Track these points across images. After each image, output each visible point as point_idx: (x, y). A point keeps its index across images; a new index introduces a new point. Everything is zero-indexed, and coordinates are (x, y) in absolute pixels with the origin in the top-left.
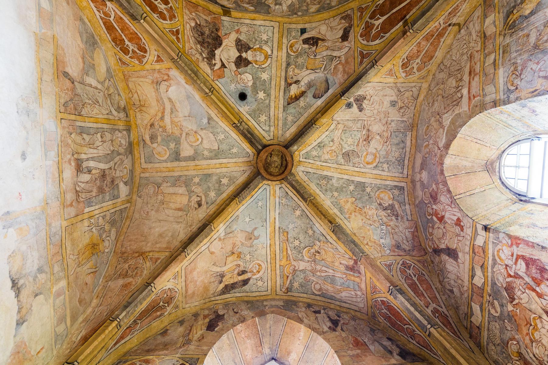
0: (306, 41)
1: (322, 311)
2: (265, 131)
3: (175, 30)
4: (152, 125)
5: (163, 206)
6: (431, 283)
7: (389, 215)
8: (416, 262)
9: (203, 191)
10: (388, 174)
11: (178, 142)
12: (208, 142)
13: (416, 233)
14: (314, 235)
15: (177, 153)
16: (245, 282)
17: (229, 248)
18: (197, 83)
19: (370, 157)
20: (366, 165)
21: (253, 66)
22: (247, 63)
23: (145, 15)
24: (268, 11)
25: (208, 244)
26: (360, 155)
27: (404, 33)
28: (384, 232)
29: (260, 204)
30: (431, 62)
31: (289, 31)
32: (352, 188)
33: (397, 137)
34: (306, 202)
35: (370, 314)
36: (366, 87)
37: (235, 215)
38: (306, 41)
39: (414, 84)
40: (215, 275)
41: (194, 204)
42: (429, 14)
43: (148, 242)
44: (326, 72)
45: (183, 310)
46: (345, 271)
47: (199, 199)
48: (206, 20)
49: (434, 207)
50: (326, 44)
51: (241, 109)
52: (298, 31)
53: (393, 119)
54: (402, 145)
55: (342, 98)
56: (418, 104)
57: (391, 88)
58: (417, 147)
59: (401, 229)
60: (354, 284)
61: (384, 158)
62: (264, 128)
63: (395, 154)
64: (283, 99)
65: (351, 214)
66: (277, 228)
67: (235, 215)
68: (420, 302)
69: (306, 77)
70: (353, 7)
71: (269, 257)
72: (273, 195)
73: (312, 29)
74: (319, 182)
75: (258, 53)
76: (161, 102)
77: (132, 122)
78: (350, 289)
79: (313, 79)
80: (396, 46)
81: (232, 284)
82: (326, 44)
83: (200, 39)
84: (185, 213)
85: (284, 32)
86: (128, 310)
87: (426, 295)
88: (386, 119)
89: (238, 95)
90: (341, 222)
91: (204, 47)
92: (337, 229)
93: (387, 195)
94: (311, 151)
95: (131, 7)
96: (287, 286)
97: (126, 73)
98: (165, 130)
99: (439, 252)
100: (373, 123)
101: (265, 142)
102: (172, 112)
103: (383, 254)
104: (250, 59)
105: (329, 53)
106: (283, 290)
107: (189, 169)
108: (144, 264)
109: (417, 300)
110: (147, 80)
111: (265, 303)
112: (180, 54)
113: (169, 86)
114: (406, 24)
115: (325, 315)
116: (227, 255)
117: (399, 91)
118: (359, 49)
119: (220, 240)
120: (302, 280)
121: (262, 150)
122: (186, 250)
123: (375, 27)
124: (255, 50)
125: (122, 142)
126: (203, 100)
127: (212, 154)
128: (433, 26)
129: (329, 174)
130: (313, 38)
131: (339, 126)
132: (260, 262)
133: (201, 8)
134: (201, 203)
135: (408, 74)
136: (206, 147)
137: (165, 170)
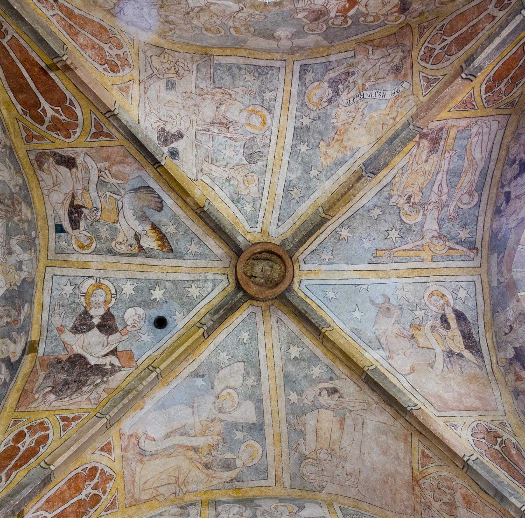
0: (75, 225)
1: (507, 189)
2: (215, 288)
3: (62, 423)
4: (207, 466)
5: (337, 450)
6: (454, 15)
8: (422, 40)
9: (311, 386)
10: (281, 90)
11: (236, 426)
12: (233, 376)
13: (376, 42)
14: (381, 206)
15: (251, 428)
16: (460, 317)
17: (405, 343)
18: (142, 391)
19: (254, 119)
20: (266, 126)
21: (113, 307)
22: (108, 316)
23: (42, 464)
24: (30, 283)
25: (398, 375)
26: (251, 136)
27: (67, 68)
28: (373, 93)
29: (331, 294)
31: (59, 251)
32: (303, 148)
33: (222, 78)
34: (327, 220)
36: (146, 127)
37: (351, 333)
38: (75, 225)
39: (142, 55)
40: (449, 366)
42: (40, 31)
43: (397, 472)
44: (123, 192)
45: (508, 414)
46: (439, 153)
47: (325, 392)
48: (45, 378)
49: (333, 14)
50: (79, 192)
52: (59, 237)
53: (194, 85)
54: (235, 70)
55: (163, 164)
56: (170, 46)
57: (147, 89)
58: (238, 45)
59: (369, 66)
60: (460, 139)
61: (255, 98)
62: (210, 290)
63: (248, 80)
64: (163, 260)
65: (345, 147)
66: (371, 267)
67: (351, 333)
68: (486, 29)
69: (129, 223)
70: (24, 151)
71: (419, 279)
72: (317, 273)
73: (56, 215)
74: (295, 201)
75: (93, 299)
76: (172, 451)
77: (204, 497)
78: (469, 145)
79: (132, 211)
80: (87, 81)
81: (464, 338)
83: (74, 387)
84: (348, 414)
85: (61, 259)
86: (507, 495)
88: (195, 97)
89: (159, 330)
90: (360, 162)
91: (87, 380)
92: (372, 168)
93: (315, 91)
94: (244, 214)
95: (32, 482)
96: (465, 249)
97: (127, 502)
98: (215, 447)
99: (404, 4)
100: (200, 117)
101: (231, 288)
102: (186, 434)
103: (409, 92)
104: (102, 311)
105: (92, 187)
106: (472, 255)
107: (276, 408)
108: (432, 476)
109: (483, 35)
110: (138, 470)
111: (495, 284)
112: (98, 415)
113: (147, 437)
114: (53, 67)
115: (512, 184)
116: (416, 346)
117: (151, 77)
118: (89, 140)
119: (390, 357)
120: (455, 224)
121: (245, 291)
122: (409, 409)
123: (56, 115)
124: (88, 304)
125: (235, 512)
126: (168, 384)
127: (252, 372)
128: (56, 27)
129: (281, 184)
130: (70, 213)
131: (206, 169)
132: (428, 293)
133: (27, 385)
134: (331, 389)
135: (126, 63)
137: (278, 448)
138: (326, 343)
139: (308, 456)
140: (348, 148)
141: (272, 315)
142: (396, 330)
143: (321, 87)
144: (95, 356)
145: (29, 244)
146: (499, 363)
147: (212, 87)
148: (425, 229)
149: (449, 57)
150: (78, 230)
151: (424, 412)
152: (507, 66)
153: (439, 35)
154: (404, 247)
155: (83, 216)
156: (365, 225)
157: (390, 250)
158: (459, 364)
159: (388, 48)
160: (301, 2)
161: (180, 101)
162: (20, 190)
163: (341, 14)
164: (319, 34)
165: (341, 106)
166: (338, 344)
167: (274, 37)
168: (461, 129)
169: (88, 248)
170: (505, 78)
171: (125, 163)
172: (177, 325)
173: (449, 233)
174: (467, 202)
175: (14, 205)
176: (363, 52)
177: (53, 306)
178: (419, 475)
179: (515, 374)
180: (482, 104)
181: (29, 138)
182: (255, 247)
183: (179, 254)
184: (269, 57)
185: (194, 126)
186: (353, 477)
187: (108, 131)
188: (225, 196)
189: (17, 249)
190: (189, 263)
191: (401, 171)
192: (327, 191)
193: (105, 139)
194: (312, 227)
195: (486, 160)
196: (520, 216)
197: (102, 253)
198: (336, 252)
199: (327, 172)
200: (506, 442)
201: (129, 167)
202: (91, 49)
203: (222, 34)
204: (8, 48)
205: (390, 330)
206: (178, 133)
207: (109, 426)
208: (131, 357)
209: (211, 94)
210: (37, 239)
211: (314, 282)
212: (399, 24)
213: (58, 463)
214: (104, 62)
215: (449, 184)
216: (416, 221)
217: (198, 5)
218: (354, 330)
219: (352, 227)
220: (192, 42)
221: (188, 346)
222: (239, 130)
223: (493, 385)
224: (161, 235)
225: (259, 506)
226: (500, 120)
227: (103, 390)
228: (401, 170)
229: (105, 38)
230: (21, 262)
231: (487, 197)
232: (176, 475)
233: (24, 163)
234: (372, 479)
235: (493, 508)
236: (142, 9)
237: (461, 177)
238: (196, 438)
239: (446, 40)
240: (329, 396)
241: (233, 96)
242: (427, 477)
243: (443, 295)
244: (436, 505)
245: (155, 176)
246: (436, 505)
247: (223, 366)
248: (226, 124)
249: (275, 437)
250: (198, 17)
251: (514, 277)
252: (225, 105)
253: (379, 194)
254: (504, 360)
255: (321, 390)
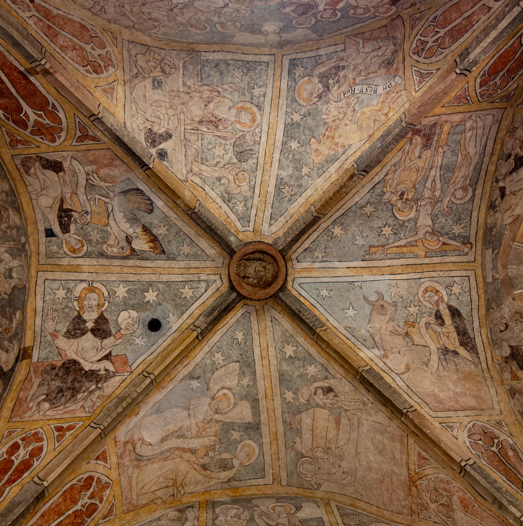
0: (65, 229)
1: (501, 184)
2: (208, 285)
3: (56, 434)
4: (204, 467)
6: (448, 5)
7: (338, 82)
8: (415, 32)
9: (306, 385)
10: (270, 86)
12: (228, 379)
13: (366, 35)
16: (455, 313)
17: (399, 341)
19: (243, 117)
20: (256, 124)
21: (106, 310)
22: (101, 320)
23: (36, 479)
24: (21, 289)
25: (393, 375)
26: (241, 133)
27: (46, 72)
29: (325, 293)
30: (90, 27)
31: (49, 255)
32: (294, 145)
33: (209, 76)
34: (319, 218)
35: (504, 105)
36: (133, 129)
38: (65, 229)
40: (444, 364)
41: (328, 400)
43: (393, 472)
44: (112, 195)
45: (505, 413)
46: (433, 148)
47: (320, 391)
48: (39, 385)
49: (321, 8)
50: (68, 196)
51: (175, 327)
52: (49, 242)
53: (181, 83)
54: (223, 67)
55: (151, 166)
56: (156, 44)
57: (132, 88)
60: (454, 134)
61: (243, 94)
62: (203, 290)
63: (237, 77)
64: (155, 262)
65: (337, 144)
66: (364, 264)
68: (481, 21)
69: (120, 226)
70: (10, 156)
71: (412, 276)
72: (311, 271)
73: (46, 219)
75: (86, 303)
76: (168, 454)
78: (463, 140)
81: (458, 335)
82: (68, 196)
83: (68, 394)
84: (343, 413)
86: (505, 503)
87: (469, 13)
88: (182, 95)
89: (153, 333)
90: (352, 159)
92: (365, 167)
93: (305, 86)
94: (236, 213)
96: (459, 244)
98: (212, 448)
100: (189, 116)
101: (225, 288)
104: (95, 315)
106: (466, 250)
107: (273, 406)
108: (428, 477)
109: (479, 27)
110: (135, 476)
111: (490, 280)
112: (92, 424)
113: (143, 442)
114: (32, 71)
115: (507, 180)
116: (411, 344)
117: (136, 76)
118: (74, 143)
123: (39, 119)
126: (163, 388)
130: (60, 217)
131: (195, 169)
133: (22, 393)
134: (326, 388)
135: (109, 63)
136: (236, 381)
137: (274, 446)
138: (319, 342)
139: (305, 455)
140: (339, 145)
141: (266, 314)
143: (311, 82)
144: (90, 361)
146: (495, 360)
147: (200, 84)
148: (418, 225)
149: (442, 51)
150: (68, 234)
151: (419, 414)
153: (432, 27)
155: (72, 219)
156: (357, 222)
157: (383, 246)
158: (454, 362)
159: (379, 41)
161: (167, 100)
162: (7, 196)
163: (330, 7)
165: (332, 102)
166: (332, 345)
167: (262, 32)
168: (454, 124)
169: (79, 252)
170: (501, 71)
171: (112, 166)
172: (171, 327)
176: (353, 45)
177: (46, 311)
178: (416, 476)
179: (511, 373)
180: (476, 98)
181: (13, 143)
182: (248, 248)
183: (171, 256)
185: (182, 125)
186: (350, 476)
187: (93, 135)
188: (216, 196)
190: (182, 264)
191: (393, 168)
192: (319, 189)
193: (91, 142)
194: (304, 226)
195: (480, 155)
196: (516, 213)
197: (94, 256)
198: (329, 250)
199: (318, 169)
200: (503, 442)
202: (72, 51)
203: (208, 30)
205: (384, 327)
210: (27, 244)
211: (307, 280)
212: (390, 16)
213: (51, 478)
214: (86, 63)
216: (409, 217)
219: (345, 225)
220: (178, 39)
221: (182, 350)
222: (229, 128)
224: (152, 237)
225: (257, 506)
226: (495, 114)
227: (98, 397)
229: (86, 38)
230: (10, 270)
231: (481, 191)
232: (174, 477)
233: (10, 168)
234: (368, 478)
235: (491, 513)
236: (123, 7)
237: (455, 172)
238: (193, 439)
239: (439, 32)
240: (324, 395)
241: (222, 94)
242: (424, 478)
243: (437, 291)
245: (143, 178)
246: (433, 506)
247: (219, 367)
249: (272, 436)
250: (183, 14)
253: (371, 191)
255: (316, 389)
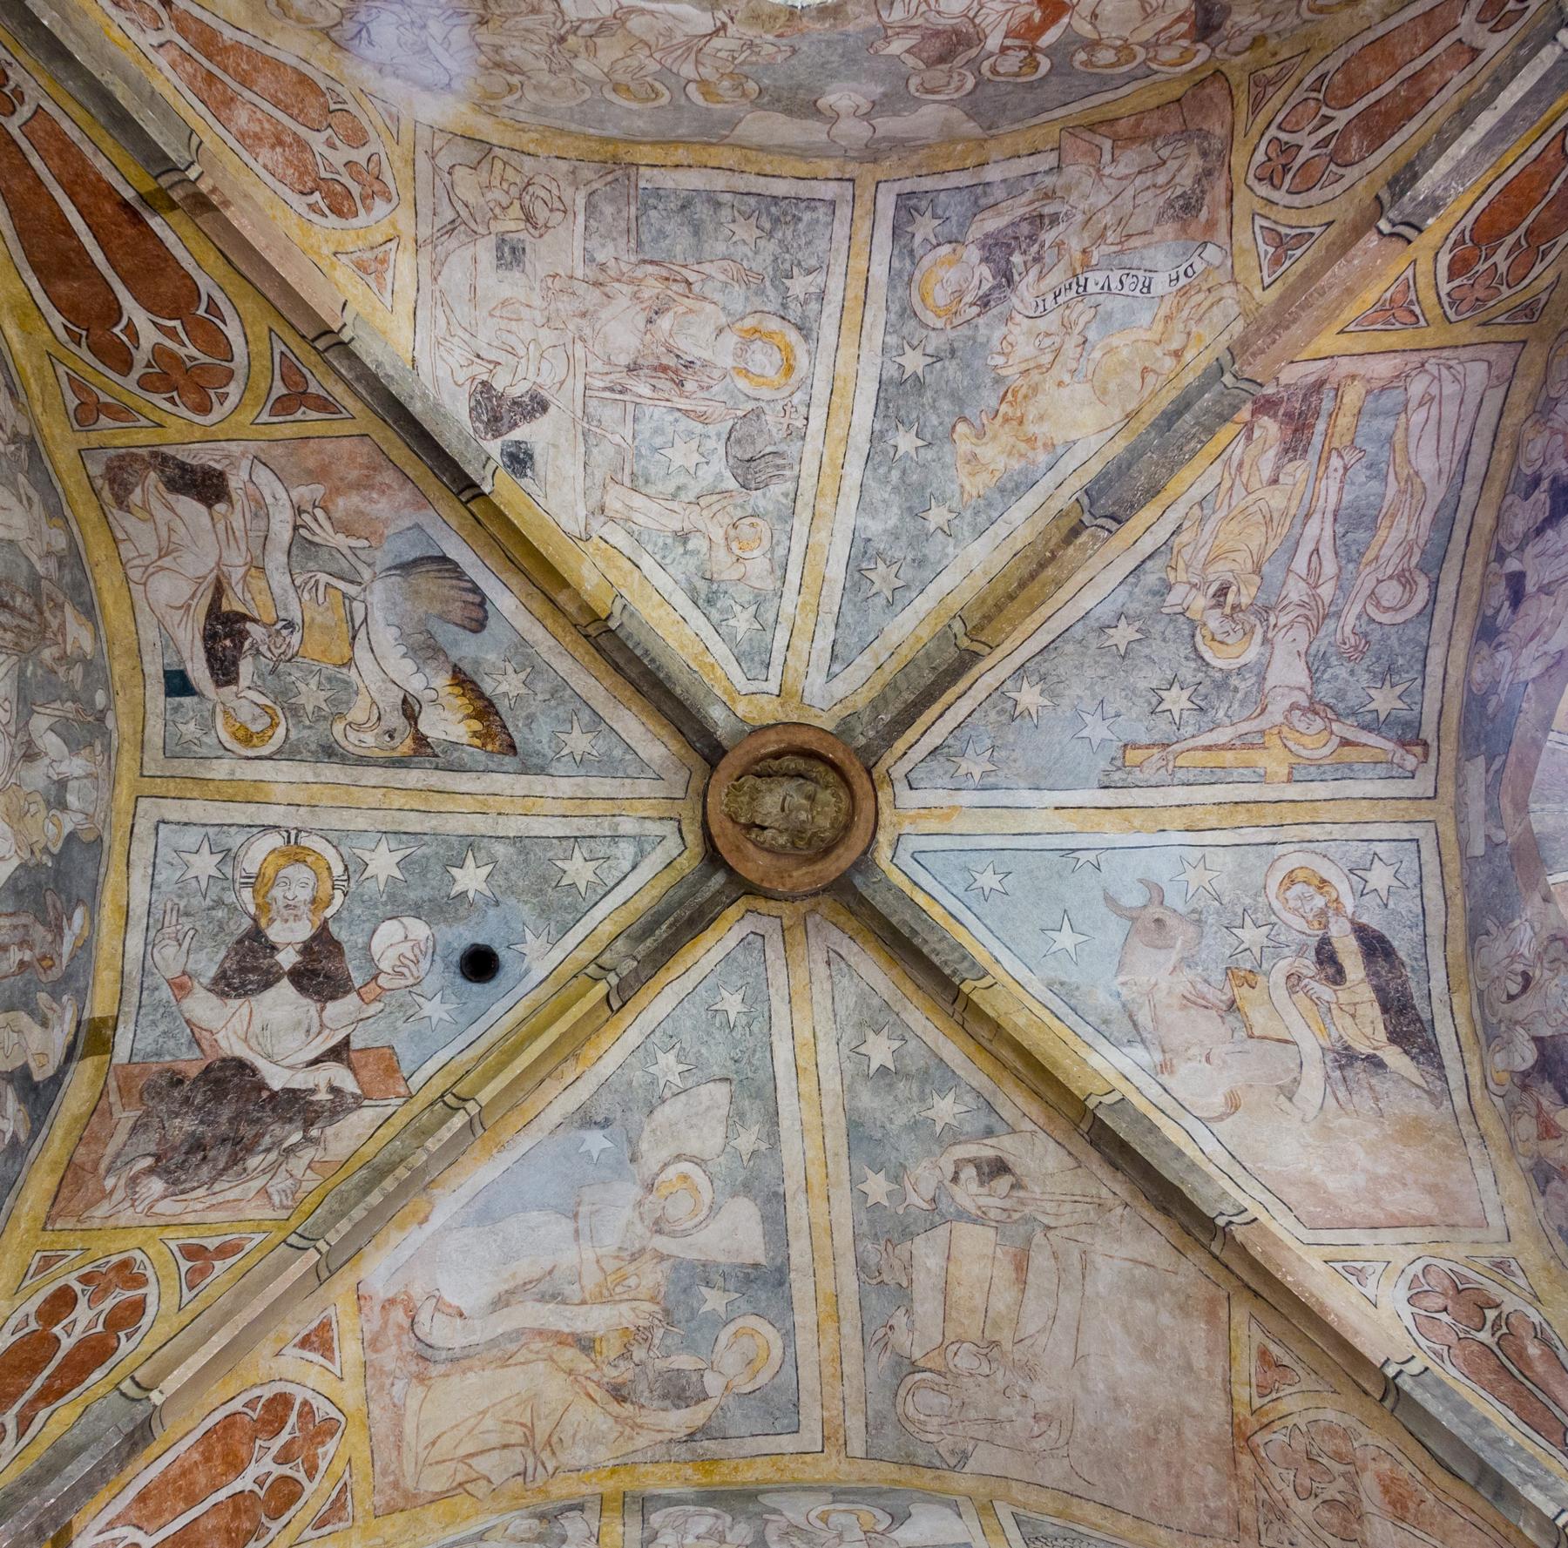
0: (224, 671)
1: (1513, 565)
2: (641, 860)
3: (185, 1265)
4: (619, 1393)
5: (1007, 1346)
6: (1357, 44)
8: (1262, 119)
9: (930, 1153)
10: (838, 269)
11: (704, 1274)
12: (697, 1124)
13: (1123, 127)
14: (1139, 617)
15: (748, 1280)
16: (1375, 946)
17: (1209, 1026)
18: (424, 1169)
19: (759, 357)
20: (796, 377)
21: (337, 917)
22: (323, 945)
23: (127, 1386)
24: (90, 845)
25: (1189, 1122)
26: (750, 405)
27: (201, 204)
28: (1115, 276)
29: (988, 880)
31: (176, 750)
32: (906, 442)
33: (662, 234)
34: (976, 656)
36: (436, 379)
37: (1047, 996)
38: (224, 671)
39: (423, 163)
40: (1342, 1093)
42: (121, 93)
43: (1186, 1410)
44: (367, 574)
45: (1518, 1237)
46: (1312, 456)
47: (969, 1172)
48: (134, 1129)
49: (993, 43)
50: (237, 575)
52: (176, 710)
53: (578, 253)
54: (702, 210)
55: (486, 489)
56: (509, 139)
57: (438, 265)
58: (712, 135)
59: (1103, 199)
60: (1375, 415)
61: (761, 292)
62: (626, 866)
63: (741, 239)
64: (488, 777)
65: (1031, 440)
66: (1107, 797)
67: (1047, 996)
68: (1451, 87)
69: (386, 668)
70: (73, 452)
71: (1250, 835)
72: (948, 817)
73: (169, 642)
74: (880, 601)
75: (277, 892)
76: (513, 1347)
77: (609, 1486)
78: (1400, 435)
79: (395, 631)
80: (258, 242)
81: (1385, 1010)
83: (222, 1155)
84: (1039, 1237)
85: (181, 774)
86: (1513, 1479)
88: (581, 288)
89: (476, 987)
90: (1075, 485)
91: (259, 1136)
92: (1110, 501)
93: (942, 272)
94: (729, 639)
95: (96, 1439)
96: (1390, 746)
97: (379, 1500)
98: (641, 1335)
99: (1208, 12)
100: (597, 349)
101: (690, 861)
102: (556, 1297)
103: (1221, 276)
104: (303, 931)
105: (276, 559)
106: (1411, 762)
107: (825, 1220)
108: (1290, 1421)
109: (1442, 104)
110: (412, 1404)
111: (1478, 848)
112: (293, 1239)
113: (440, 1306)
114: (160, 201)
115: (1530, 551)
116: (1243, 1034)
117: (451, 229)
118: (264, 417)
119: (1165, 1067)
120: (1359, 670)
121: (731, 871)
122: (1221, 1221)
123: (168, 343)
124: (263, 908)
125: (702, 1529)
126: (502, 1147)
127: (753, 1111)
128: (168, 80)
129: (840, 551)
130: (210, 637)
131: (614, 504)
132: (1279, 875)
133: (82, 1150)
134: (989, 1162)
135: (375, 188)
137: (830, 1339)
138: (972, 1026)
139: (921, 1363)
140: (1039, 444)
141: (812, 941)
142: (1183, 988)
143: (959, 260)
144: (284, 1063)
145: (88, 730)
146: (1492, 1086)
147: (633, 259)
148: (1269, 684)
149: (1341, 171)
150: (234, 688)
151: (1265, 1232)
152: (1515, 199)
153: (1312, 103)
154: (1206, 739)
155: (247, 644)
156: (1089, 673)
157: (1166, 746)
158: (1371, 1088)
159: (1159, 143)
160: (898, 5)
161: (537, 302)
162: (61, 566)
163: (1018, 42)
164: (952, 103)
165: (1018, 318)
166: (1009, 1028)
167: (818, 111)
168: (1376, 384)
169: (263, 742)
170: (1510, 232)
171: (372, 487)
172: (527, 971)
173: (1341, 695)
174: (1396, 605)
175: (41, 613)
176: (1084, 154)
177: (159, 916)
178: (1252, 1419)
179: (1538, 1117)
180: (1439, 311)
181: (88, 412)
182: (763, 740)
183: (535, 760)
184: (803, 169)
185: (580, 377)
186: (1055, 1425)
187: (322, 393)
188: (671, 585)
189: (51, 743)
190: (565, 787)
191: (1196, 510)
192: (978, 571)
193: (315, 415)
194: (932, 677)
195: (1450, 480)
196: (1553, 647)
197: (306, 755)
198: (1003, 753)
199: (977, 513)
200: (1512, 1320)
201: (384, 500)
202: (273, 147)
203: (664, 100)
204: (25, 145)
205: (1163, 985)
206: (532, 398)
207: (324, 1274)
208: (390, 1066)
209: (631, 282)
210: (110, 715)
211: (937, 843)
212: (1192, 71)
213: (172, 1383)
214: (310, 184)
215: (1341, 550)
216: (1242, 661)
217: (593, 15)
218: (1056, 987)
219: (1052, 679)
220: (573, 127)
221: (563, 1035)
222: (715, 389)
223: (1473, 1151)
224: (480, 704)
225: (775, 1511)
226: (1493, 357)
227: (309, 1167)
228: (1196, 509)
229: (314, 114)
230: (62, 784)
231: (1453, 588)
232: (527, 1420)
233: (72, 487)
234: (1110, 1432)
235: (1473, 1518)
236: (424, 27)
237: (1377, 529)
238: (585, 1307)
239: (1332, 119)
240: (982, 1184)
241: (696, 288)
242: (1276, 1426)
243: (1324, 881)
244: (1302, 1509)
245: (462, 526)
246: (1301, 1508)
247: (667, 1093)
248: (674, 371)
249: (822, 1307)
250: (592, 51)
251: (1536, 828)
252: (671, 314)
253: (1131, 579)
254: (1506, 1075)
255: (959, 1165)
